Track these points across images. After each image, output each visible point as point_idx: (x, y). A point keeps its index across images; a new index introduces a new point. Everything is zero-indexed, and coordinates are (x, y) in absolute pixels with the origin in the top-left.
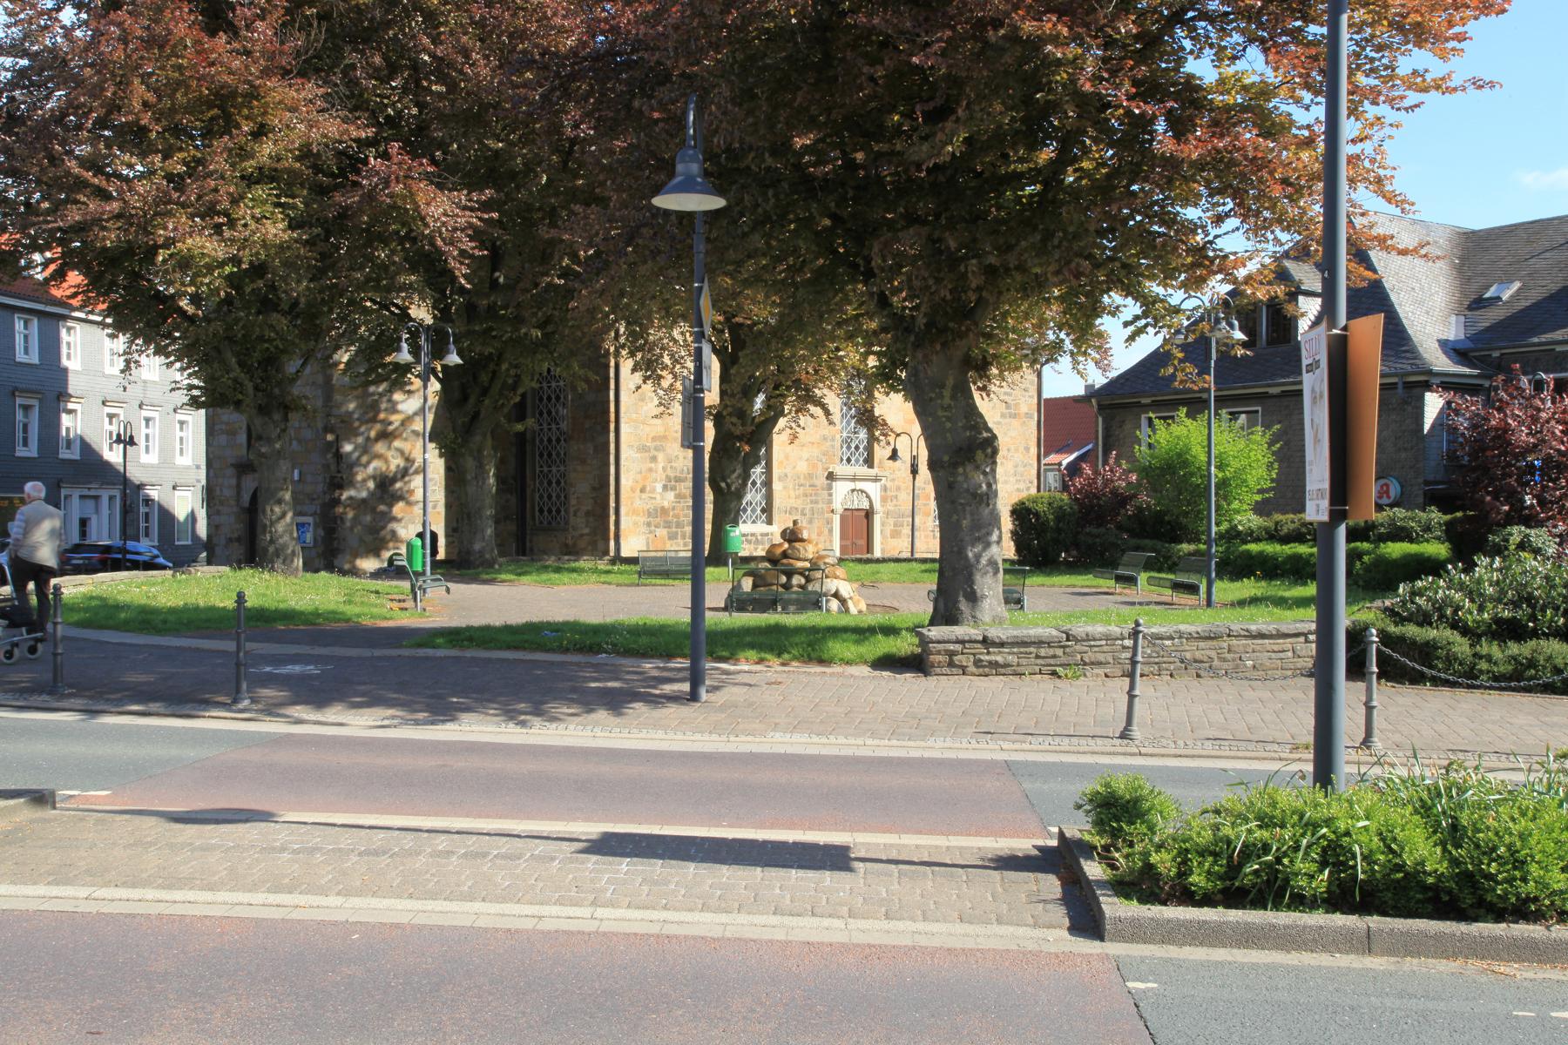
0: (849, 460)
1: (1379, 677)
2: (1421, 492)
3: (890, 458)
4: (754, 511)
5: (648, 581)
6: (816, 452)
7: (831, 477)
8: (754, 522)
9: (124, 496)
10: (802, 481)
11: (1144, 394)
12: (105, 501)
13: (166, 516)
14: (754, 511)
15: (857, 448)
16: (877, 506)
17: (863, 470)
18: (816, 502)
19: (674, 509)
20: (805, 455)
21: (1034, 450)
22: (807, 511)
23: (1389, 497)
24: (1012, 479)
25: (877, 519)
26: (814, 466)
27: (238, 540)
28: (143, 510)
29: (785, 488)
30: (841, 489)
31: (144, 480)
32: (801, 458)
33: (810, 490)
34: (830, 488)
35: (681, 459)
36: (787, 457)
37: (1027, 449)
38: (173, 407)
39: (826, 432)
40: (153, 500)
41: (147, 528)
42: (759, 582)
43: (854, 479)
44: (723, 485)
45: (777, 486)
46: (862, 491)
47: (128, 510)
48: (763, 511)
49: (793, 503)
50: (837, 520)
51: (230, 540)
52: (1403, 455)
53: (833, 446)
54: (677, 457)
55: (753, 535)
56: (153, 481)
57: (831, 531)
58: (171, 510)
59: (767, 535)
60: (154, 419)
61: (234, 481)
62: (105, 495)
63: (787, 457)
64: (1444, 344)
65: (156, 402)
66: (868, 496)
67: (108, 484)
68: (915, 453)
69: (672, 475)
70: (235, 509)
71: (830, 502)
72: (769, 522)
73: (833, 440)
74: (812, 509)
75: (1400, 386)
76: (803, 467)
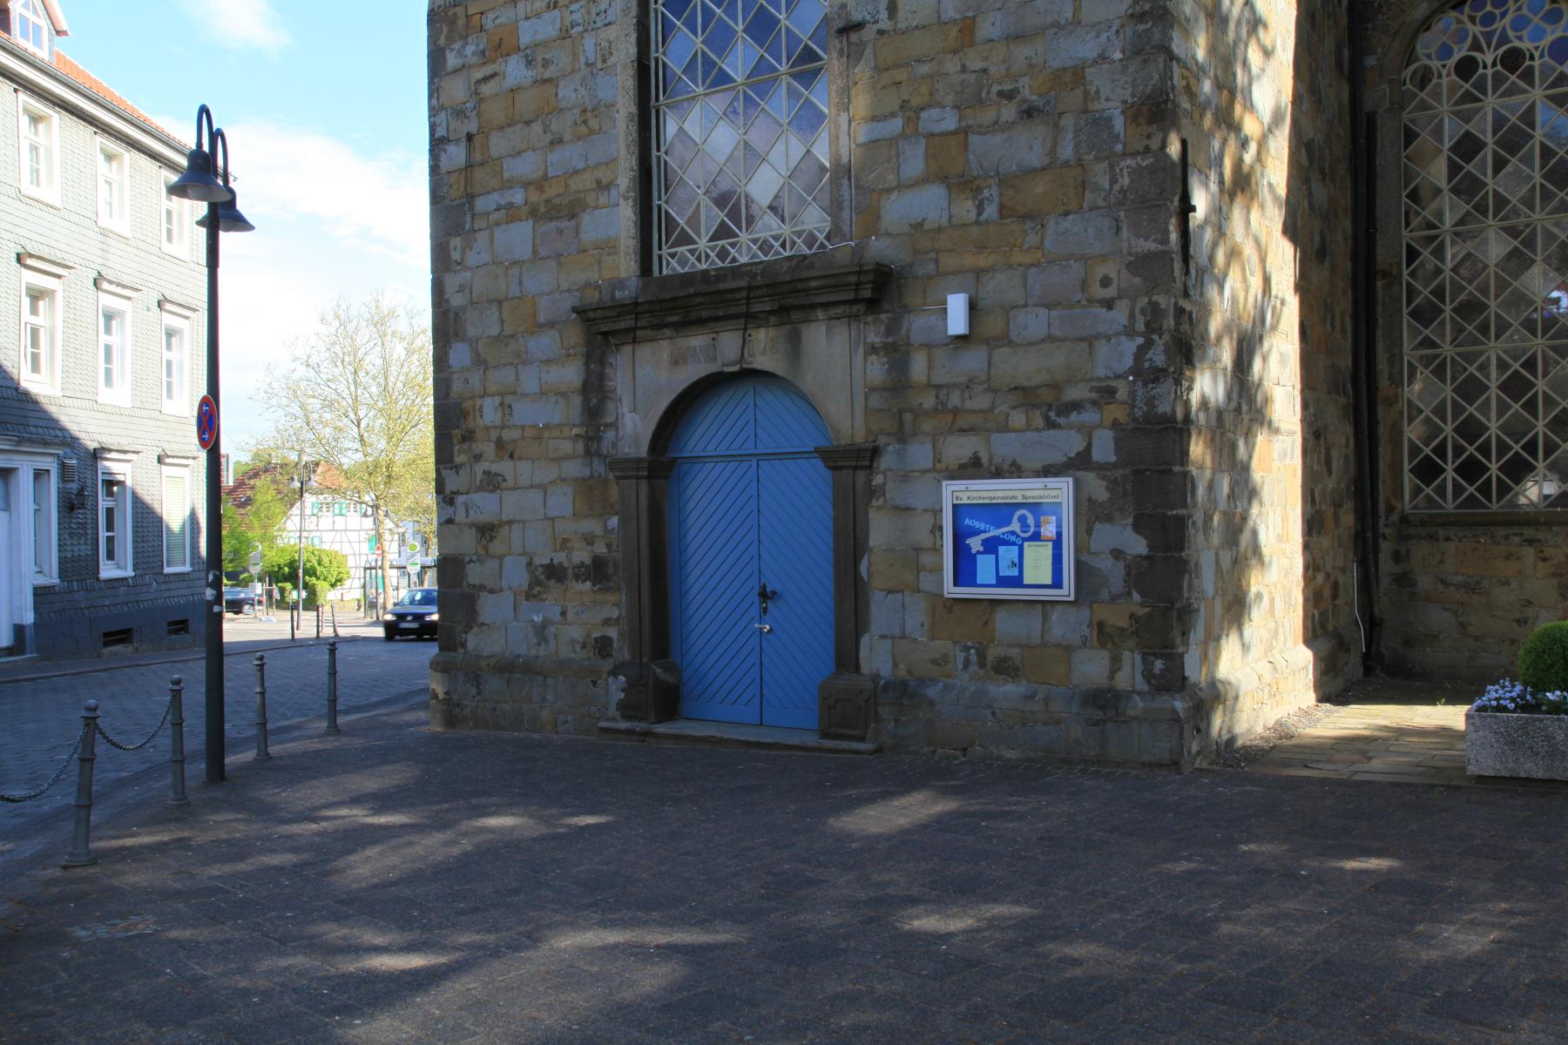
1: (304, 609)
9: (65, 472)
12: (25, 479)
13: (147, 520)
27: (597, 571)
28: (103, 503)
31: (108, 441)
38: (156, 297)
40: (121, 483)
41: (110, 540)
47: (75, 505)
51: (555, 572)
56: (124, 443)
58: (156, 507)
60: (121, 314)
61: (571, 374)
62: (25, 468)
64: (1203, 397)
65: (126, 280)
67: (32, 442)
70: (575, 469)
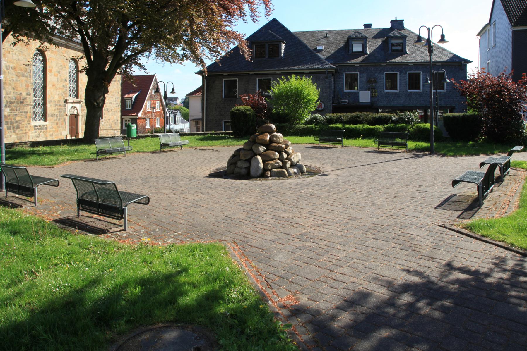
0: (70, 95)
2: (331, 106)
3: (171, 93)
4: (39, 116)
5: (102, 157)
6: (61, 91)
7: (66, 101)
8: (39, 121)
10: (57, 103)
11: (225, 72)
14: (39, 116)
15: (73, 91)
16: (80, 113)
17: (75, 99)
18: (61, 112)
19: (9, 116)
20: (58, 93)
21: (120, 93)
22: (58, 116)
23: (321, 107)
24: (115, 103)
25: (80, 117)
26: (60, 97)
29: (51, 106)
30: (69, 106)
32: (56, 94)
33: (59, 107)
34: (65, 106)
35: (12, 93)
36: (51, 94)
37: (118, 92)
39: (64, 84)
42: (266, 159)
43: (73, 103)
44: (95, 104)
45: (48, 105)
46: (75, 107)
48: (42, 116)
49: (55, 112)
50: (67, 118)
52: (325, 94)
53: (66, 90)
54: (11, 92)
55: (40, 126)
57: (66, 123)
59: (45, 126)
63: (51, 94)
66: (77, 109)
68: (166, 90)
69: (9, 100)
71: (65, 112)
72: (45, 120)
73: (66, 87)
74: (60, 115)
75: (327, 73)
76: (57, 98)
